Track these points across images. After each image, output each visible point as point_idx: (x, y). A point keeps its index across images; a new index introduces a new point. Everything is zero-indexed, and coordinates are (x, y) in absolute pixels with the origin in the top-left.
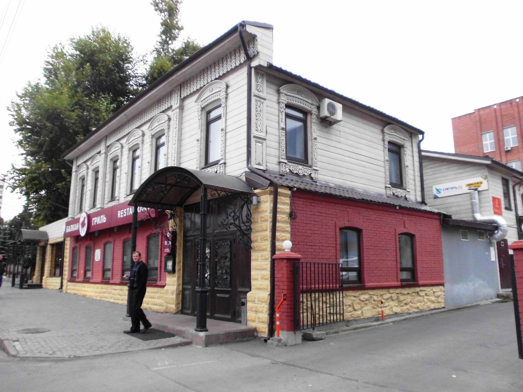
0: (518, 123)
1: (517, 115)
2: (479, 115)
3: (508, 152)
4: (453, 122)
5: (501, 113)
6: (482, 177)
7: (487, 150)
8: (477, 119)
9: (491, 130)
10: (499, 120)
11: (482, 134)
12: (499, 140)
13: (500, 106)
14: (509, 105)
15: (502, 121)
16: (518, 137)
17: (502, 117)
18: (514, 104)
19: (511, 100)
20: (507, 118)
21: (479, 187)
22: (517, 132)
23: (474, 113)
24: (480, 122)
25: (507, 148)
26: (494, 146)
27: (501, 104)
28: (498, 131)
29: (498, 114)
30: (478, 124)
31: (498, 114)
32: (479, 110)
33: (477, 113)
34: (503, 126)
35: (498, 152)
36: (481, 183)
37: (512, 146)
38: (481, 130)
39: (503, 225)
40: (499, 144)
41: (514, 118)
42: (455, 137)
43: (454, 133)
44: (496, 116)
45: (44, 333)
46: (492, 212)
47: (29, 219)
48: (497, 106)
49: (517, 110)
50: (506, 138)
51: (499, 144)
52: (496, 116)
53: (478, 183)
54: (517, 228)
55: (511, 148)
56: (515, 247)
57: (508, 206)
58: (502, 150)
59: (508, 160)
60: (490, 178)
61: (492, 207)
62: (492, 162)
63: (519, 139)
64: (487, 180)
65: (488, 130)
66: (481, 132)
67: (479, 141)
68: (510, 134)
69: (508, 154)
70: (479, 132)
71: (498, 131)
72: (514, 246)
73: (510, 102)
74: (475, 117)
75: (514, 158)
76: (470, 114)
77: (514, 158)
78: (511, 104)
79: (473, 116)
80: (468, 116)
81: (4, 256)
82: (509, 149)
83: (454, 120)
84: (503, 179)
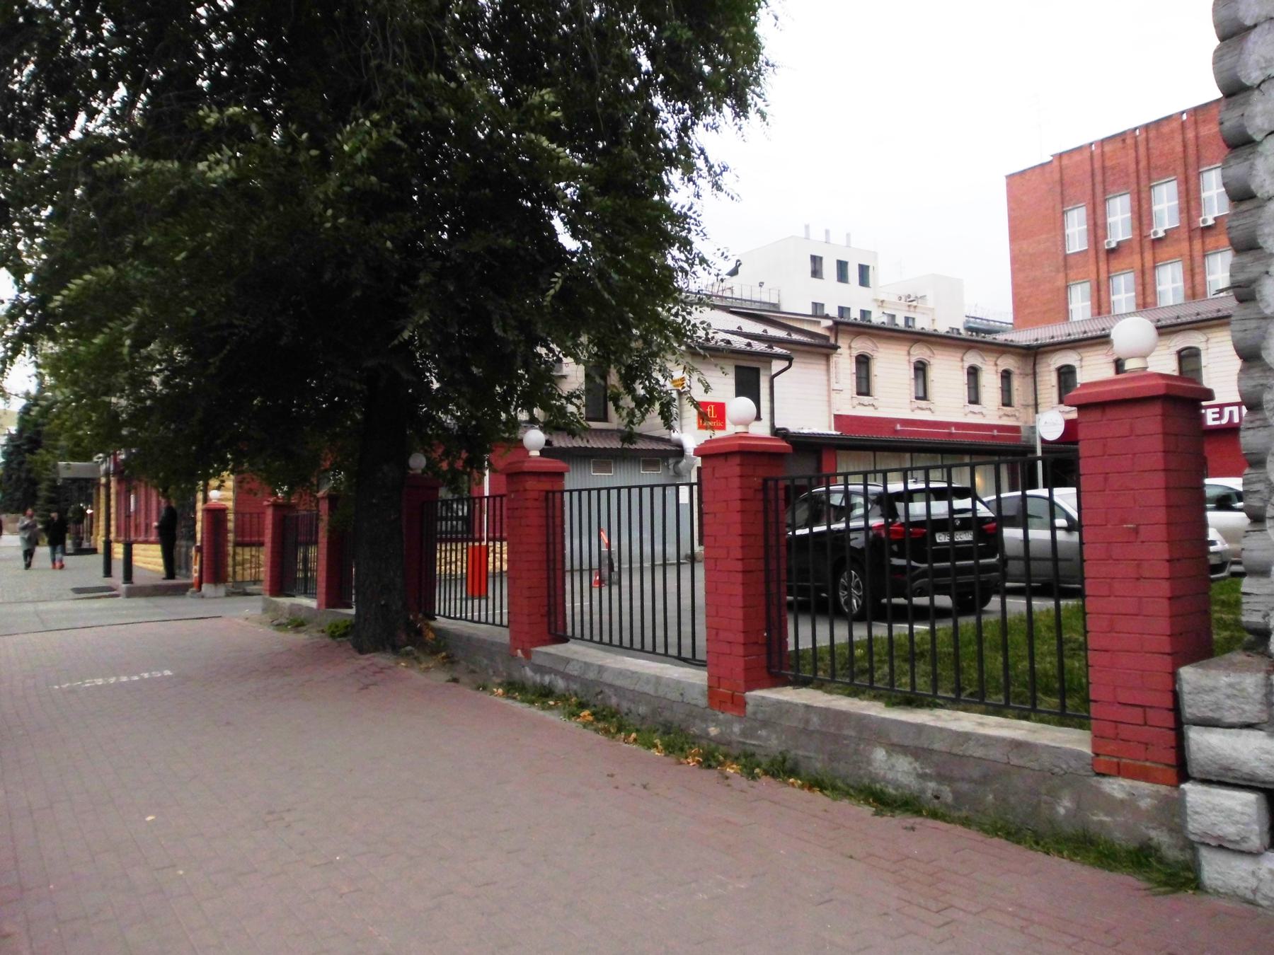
0: (1134, 186)
1: (1132, 167)
3: (1111, 252)
4: (1008, 185)
5: (1103, 161)
8: (1057, 176)
9: (1170, 176)
10: (1099, 178)
11: (1151, 187)
13: (1102, 148)
14: (1120, 145)
15: (1104, 181)
17: (1104, 173)
18: (1129, 141)
22: (1132, 207)
24: (1062, 183)
25: (1204, 221)
26: (1176, 214)
27: (1103, 142)
28: (1094, 204)
29: (1097, 165)
30: (1058, 189)
32: (1060, 156)
33: (1056, 163)
34: (1105, 192)
35: (1092, 253)
38: (1063, 203)
41: (1127, 175)
42: (1011, 219)
44: (1093, 170)
47: (255, 408)
49: (1133, 155)
52: (1093, 170)
55: (1215, 219)
56: (708, 452)
59: (1111, 269)
65: (1075, 203)
66: (1198, 168)
67: (1060, 226)
68: (1165, 198)
69: (1112, 256)
70: (1058, 206)
71: (1094, 204)
72: (705, 449)
73: (1122, 137)
76: (1042, 165)
77: (1124, 266)
78: (1124, 141)
79: (1048, 169)
81: (43, 11)
83: (1010, 178)
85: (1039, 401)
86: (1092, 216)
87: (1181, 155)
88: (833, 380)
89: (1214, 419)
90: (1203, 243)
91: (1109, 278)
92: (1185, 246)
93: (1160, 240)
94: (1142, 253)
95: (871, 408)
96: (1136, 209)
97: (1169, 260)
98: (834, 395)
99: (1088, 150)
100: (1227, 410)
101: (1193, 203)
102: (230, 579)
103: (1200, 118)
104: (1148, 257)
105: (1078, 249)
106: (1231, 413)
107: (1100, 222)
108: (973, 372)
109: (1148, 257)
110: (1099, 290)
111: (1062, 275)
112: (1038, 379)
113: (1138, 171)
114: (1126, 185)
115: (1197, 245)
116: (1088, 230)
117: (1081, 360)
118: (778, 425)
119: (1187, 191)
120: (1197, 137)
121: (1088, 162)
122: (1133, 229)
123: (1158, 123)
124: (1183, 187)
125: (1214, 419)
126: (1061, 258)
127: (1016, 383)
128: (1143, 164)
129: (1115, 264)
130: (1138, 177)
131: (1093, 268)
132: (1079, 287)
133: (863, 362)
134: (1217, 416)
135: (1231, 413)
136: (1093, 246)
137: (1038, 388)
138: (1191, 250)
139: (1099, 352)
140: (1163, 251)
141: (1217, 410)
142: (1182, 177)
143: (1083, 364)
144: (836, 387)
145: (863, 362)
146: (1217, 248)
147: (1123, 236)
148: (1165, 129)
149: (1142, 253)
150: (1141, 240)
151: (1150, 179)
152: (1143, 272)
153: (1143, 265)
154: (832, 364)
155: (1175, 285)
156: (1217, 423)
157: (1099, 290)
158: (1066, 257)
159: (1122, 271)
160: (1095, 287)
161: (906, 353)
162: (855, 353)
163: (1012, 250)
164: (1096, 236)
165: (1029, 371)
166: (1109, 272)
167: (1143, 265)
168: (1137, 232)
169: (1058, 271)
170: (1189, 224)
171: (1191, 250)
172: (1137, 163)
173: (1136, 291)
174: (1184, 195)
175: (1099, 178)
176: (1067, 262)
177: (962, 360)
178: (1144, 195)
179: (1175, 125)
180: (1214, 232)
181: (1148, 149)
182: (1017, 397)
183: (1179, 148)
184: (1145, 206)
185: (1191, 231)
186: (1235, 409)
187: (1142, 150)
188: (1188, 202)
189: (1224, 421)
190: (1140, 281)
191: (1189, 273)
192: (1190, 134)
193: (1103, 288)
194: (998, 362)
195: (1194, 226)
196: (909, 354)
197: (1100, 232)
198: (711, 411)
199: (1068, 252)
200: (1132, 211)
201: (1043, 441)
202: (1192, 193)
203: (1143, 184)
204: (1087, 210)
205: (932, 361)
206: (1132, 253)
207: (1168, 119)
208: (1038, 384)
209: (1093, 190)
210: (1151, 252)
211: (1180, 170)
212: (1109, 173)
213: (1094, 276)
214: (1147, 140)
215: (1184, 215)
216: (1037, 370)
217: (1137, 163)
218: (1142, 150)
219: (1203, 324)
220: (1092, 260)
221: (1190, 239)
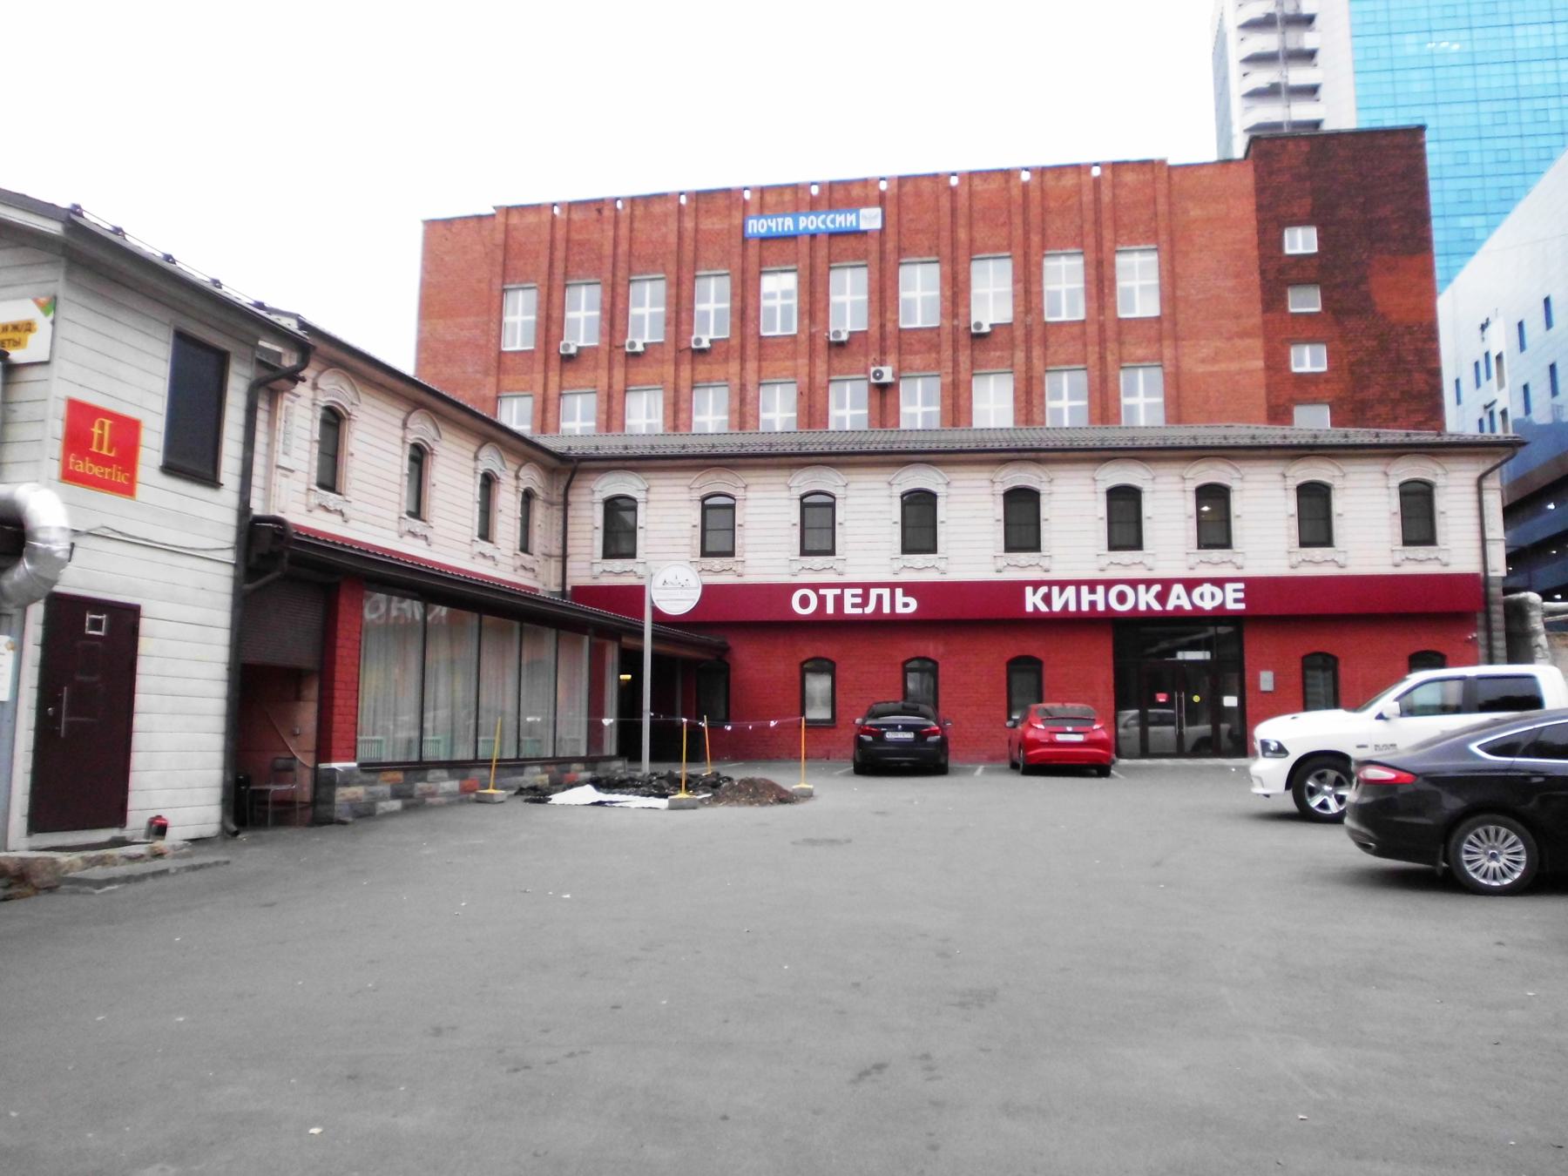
2: (507, 225)
3: (567, 359)
5: (568, 232)
6: (36, 301)
7: (514, 343)
8: (499, 237)
9: (655, 272)
10: (560, 254)
12: (548, 318)
14: (594, 214)
15: (567, 259)
16: (602, 319)
17: (568, 249)
18: (607, 213)
19: (602, 201)
20: (582, 253)
21: (17, 344)
22: (602, 302)
23: (493, 216)
24: (506, 247)
26: (532, 338)
27: (571, 206)
29: (560, 233)
30: (500, 257)
31: (560, 233)
32: (508, 210)
33: (501, 219)
34: (566, 274)
35: (540, 356)
36: (29, 327)
37: (581, 344)
39: (47, 528)
40: (547, 330)
41: (600, 258)
43: (426, 270)
45: (596, 801)
46: (55, 468)
48: (562, 210)
49: (611, 234)
50: (569, 315)
51: (547, 330)
53: (16, 328)
54: (235, 566)
55: (711, 341)
57: (413, 509)
58: (554, 351)
59: (565, 384)
60: (67, 310)
61: (55, 448)
62: (67, 230)
63: (603, 323)
64: (51, 317)
65: (524, 280)
66: (504, 283)
69: (568, 366)
70: (497, 281)
73: (598, 205)
74: (493, 230)
75: (582, 382)
76: (480, 218)
77: (582, 382)
78: (599, 211)
79: (487, 224)
80: (472, 224)
82: (573, 350)
83: (431, 225)
84: (182, 339)
85: (569, 550)
86: (544, 306)
87: (674, 247)
88: (279, 447)
89: (854, 605)
90: (693, 369)
91: (561, 395)
92: (669, 370)
93: (636, 355)
94: (610, 369)
95: (338, 518)
96: (608, 306)
97: (647, 385)
98: (278, 477)
99: (550, 213)
100: (874, 592)
101: (684, 315)
102: (316, 488)
103: (703, 206)
104: (619, 374)
105: (518, 347)
106: (880, 597)
107: (555, 314)
108: (488, 481)
109: (619, 374)
110: (544, 411)
111: (492, 380)
112: (570, 513)
113: (615, 255)
114: (597, 272)
115: (686, 372)
116: (538, 324)
117: (647, 490)
118: (257, 508)
119: (678, 297)
120: (697, 230)
121: (548, 226)
122: (602, 333)
123: (648, 200)
124: (673, 291)
125: (854, 605)
126: (493, 354)
127: (539, 513)
128: (623, 248)
129: (570, 377)
130: (614, 265)
131: (539, 378)
132: (515, 402)
133: (333, 421)
134: (859, 600)
135: (880, 597)
136: (543, 347)
137: (570, 528)
138: (677, 376)
139: (774, 480)
140: (641, 372)
141: (859, 591)
142: (673, 278)
143: (651, 497)
144: (284, 461)
145: (333, 421)
146: (709, 380)
147: (586, 340)
148: (657, 209)
149: (610, 369)
150: (611, 351)
151: (630, 271)
152: (610, 397)
153: (610, 386)
154: (281, 414)
155: (649, 421)
156: (859, 611)
157: (544, 411)
158: (501, 353)
159: (577, 389)
160: (540, 405)
161: (399, 423)
162: (323, 400)
163: (420, 331)
164: (547, 336)
165: (557, 496)
166: (561, 387)
167: (610, 386)
168: (607, 339)
169: (486, 373)
170: (677, 341)
171: (677, 376)
172: (616, 245)
173: (598, 420)
174: (674, 301)
175: (560, 254)
176: (501, 362)
177: (476, 458)
178: (620, 290)
179: (671, 207)
180: (709, 359)
181: (631, 230)
182: (538, 541)
183: (673, 239)
184: (620, 306)
185: (679, 351)
186: (886, 592)
187: (624, 230)
188: (678, 313)
189: (870, 609)
190: (605, 407)
191: (671, 408)
192: (689, 224)
193: (551, 408)
194: (521, 474)
195: (684, 345)
196: (405, 426)
197: (554, 329)
198: (101, 431)
199: (504, 349)
200: (602, 309)
201: (656, 611)
202: (684, 302)
203: (621, 274)
204: (539, 295)
205: (437, 448)
206: (596, 368)
207: (662, 197)
208: (570, 521)
209: (551, 265)
210: (623, 370)
211: (672, 267)
212: (575, 250)
213: (539, 389)
214: (632, 218)
215: (672, 329)
216: (571, 498)
217: (616, 245)
218: (624, 230)
219: (940, 457)
220: (539, 367)
221: (677, 364)
